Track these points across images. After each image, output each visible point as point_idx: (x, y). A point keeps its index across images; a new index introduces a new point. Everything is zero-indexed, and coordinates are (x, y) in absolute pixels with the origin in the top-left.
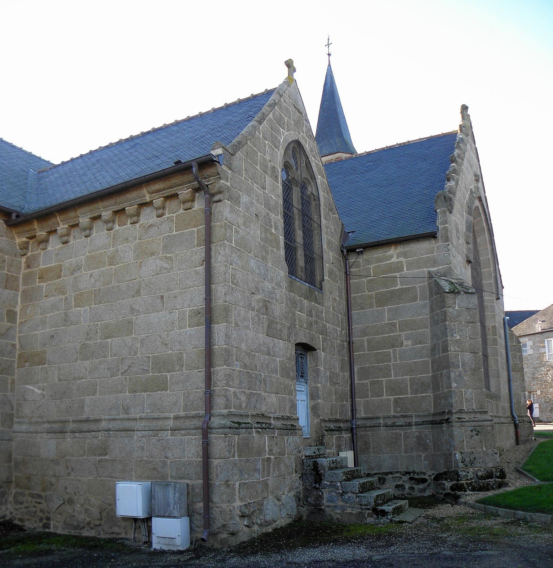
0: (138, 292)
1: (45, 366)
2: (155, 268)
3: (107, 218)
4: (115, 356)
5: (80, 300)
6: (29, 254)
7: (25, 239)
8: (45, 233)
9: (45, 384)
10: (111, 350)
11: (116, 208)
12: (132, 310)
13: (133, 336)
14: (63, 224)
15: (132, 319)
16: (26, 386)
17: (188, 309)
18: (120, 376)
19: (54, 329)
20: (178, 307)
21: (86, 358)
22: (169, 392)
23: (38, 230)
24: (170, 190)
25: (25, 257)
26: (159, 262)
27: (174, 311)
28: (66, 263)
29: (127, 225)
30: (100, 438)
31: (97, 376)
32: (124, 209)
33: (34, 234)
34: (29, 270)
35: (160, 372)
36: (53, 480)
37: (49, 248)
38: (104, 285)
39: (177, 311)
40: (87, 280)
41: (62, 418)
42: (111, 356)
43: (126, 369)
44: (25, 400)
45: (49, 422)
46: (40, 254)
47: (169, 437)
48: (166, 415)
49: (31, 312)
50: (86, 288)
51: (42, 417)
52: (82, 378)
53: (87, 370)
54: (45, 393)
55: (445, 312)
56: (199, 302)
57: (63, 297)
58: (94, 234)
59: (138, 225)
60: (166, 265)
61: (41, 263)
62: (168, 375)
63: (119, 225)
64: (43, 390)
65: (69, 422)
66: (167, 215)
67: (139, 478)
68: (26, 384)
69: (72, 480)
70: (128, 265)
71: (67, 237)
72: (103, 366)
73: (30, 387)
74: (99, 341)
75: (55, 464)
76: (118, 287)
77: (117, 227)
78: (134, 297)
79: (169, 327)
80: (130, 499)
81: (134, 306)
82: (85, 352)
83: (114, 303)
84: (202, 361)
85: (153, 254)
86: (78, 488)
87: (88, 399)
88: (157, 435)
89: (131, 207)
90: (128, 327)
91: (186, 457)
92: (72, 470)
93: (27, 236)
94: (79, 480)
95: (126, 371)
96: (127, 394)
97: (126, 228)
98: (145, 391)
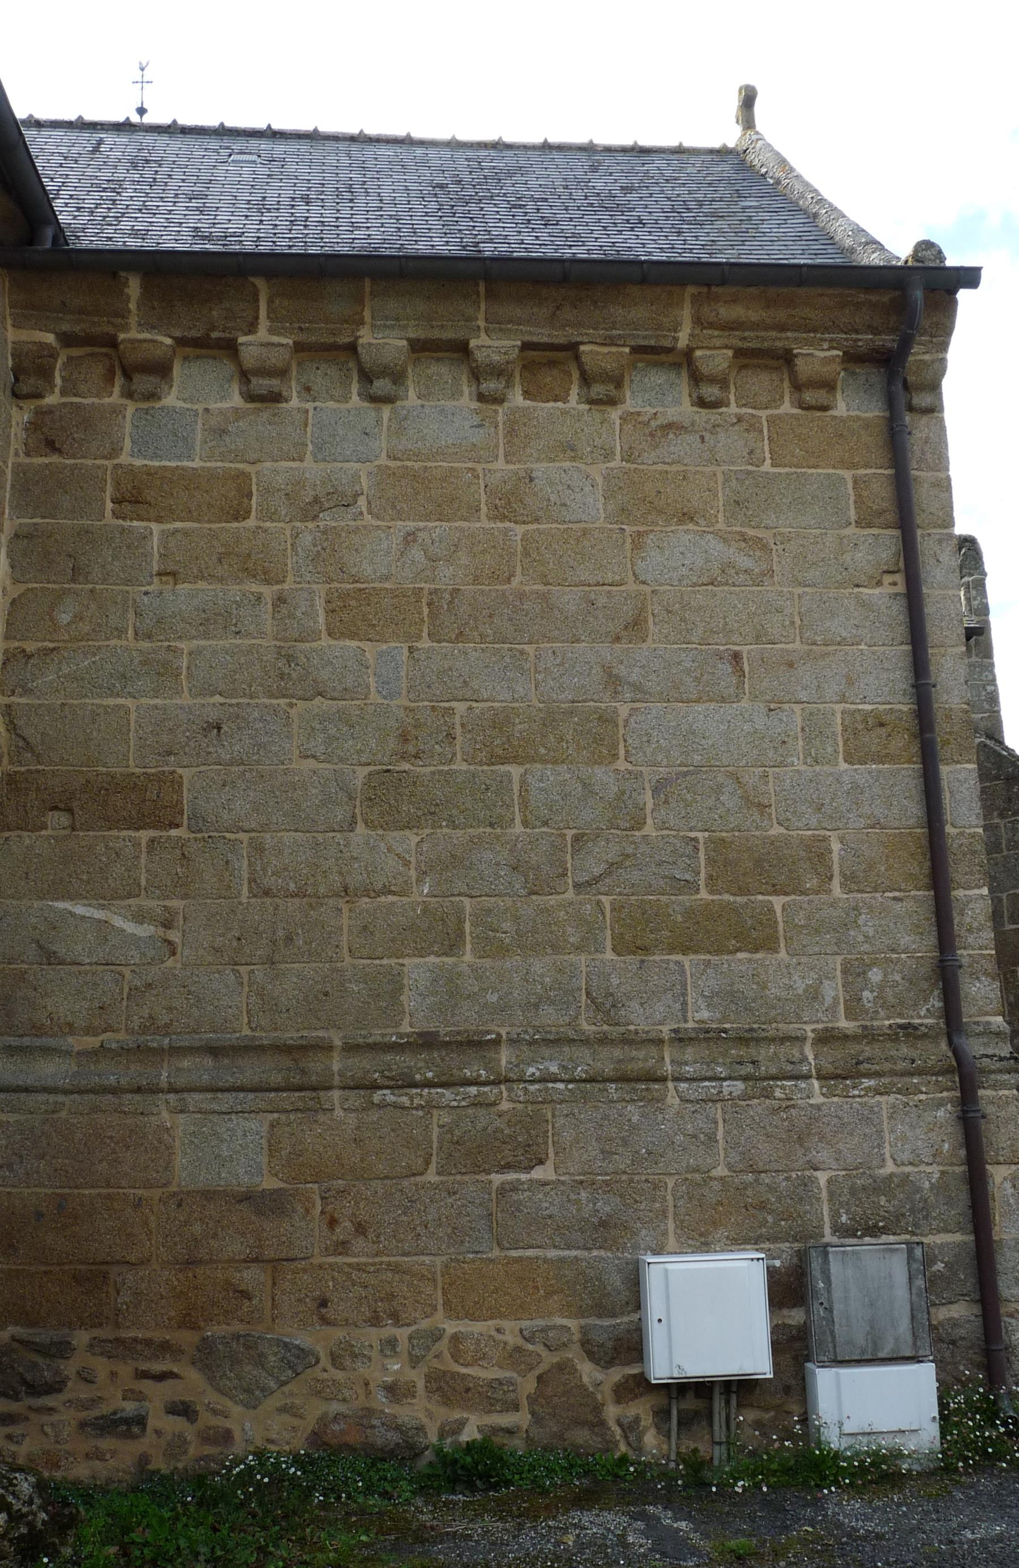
0: (636, 626)
1: (174, 832)
2: (700, 563)
3: (496, 358)
4: (546, 823)
5: (355, 612)
6: (52, 399)
7: (50, 338)
8: (169, 341)
9: (175, 903)
10: (525, 804)
11: (543, 335)
12: (613, 681)
13: (622, 765)
14: (271, 331)
15: (615, 711)
16: (61, 905)
17: (839, 708)
18: (570, 894)
19: (218, 699)
20: (803, 696)
21: (392, 821)
22: (783, 954)
23: (133, 320)
24: (774, 334)
25: (31, 405)
26: (715, 546)
27: (786, 706)
28: (273, 471)
29: (565, 401)
30: (505, 1106)
31: (460, 886)
32: (572, 348)
33: (110, 329)
34: (55, 459)
35: (742, 891)
36: (251, 1276)
37: (171, 400)
38: (476, 580)
39: (797, 708)
40: (382, 552)
41: (291, 1036)
42: (525, 823)
43: (597, 871)
44: (51, 958)
45: (214, 1051)
46: (117, 411)
47: (818, 1100)
48: (792, 1029)
49: (78, 618)
50: (387, 578)
51: (166, 1030)
52: (387, 891)
53: (407, 864)
54: (174, 936)
55: (985, 820)
56: (884, 688)
57: (268, 592)
58: (412, 398)
59: (615, 414)
60: (744, 562)
61: (128, 444)
62: (778, 902)
63: (527, 394)
64: (167, 925)
65: (331, 1048)
66: (733, 409)
67: (738, 1242)
68: (63, 898)
69: (359, 1268)
70: (585, 532)
71: (275, 382)
72: (488, 855)
73: (80, 910)
74: (464, 767)
75: (259, 1213)
76: (544, 597)
77: (517, 398)
78: (618, 639)
79: (771, 753)
80: (708, 1312)
81: (622, 670)
82: (389, 799)
83: (530, 649)
84: (919, 868)
85: (687, 517)
86: (391, 1296)
87: (417, 969)
88: (768, 1094)
89: (605, 350)
90: (602, 737)
91: (889, 1162)
92: (361, 1229)
93: (65, 327)
94: (396, 1269)
95: (597, 879)
96: (609, 955)
97: (564, 413)
98: (685, 951)
